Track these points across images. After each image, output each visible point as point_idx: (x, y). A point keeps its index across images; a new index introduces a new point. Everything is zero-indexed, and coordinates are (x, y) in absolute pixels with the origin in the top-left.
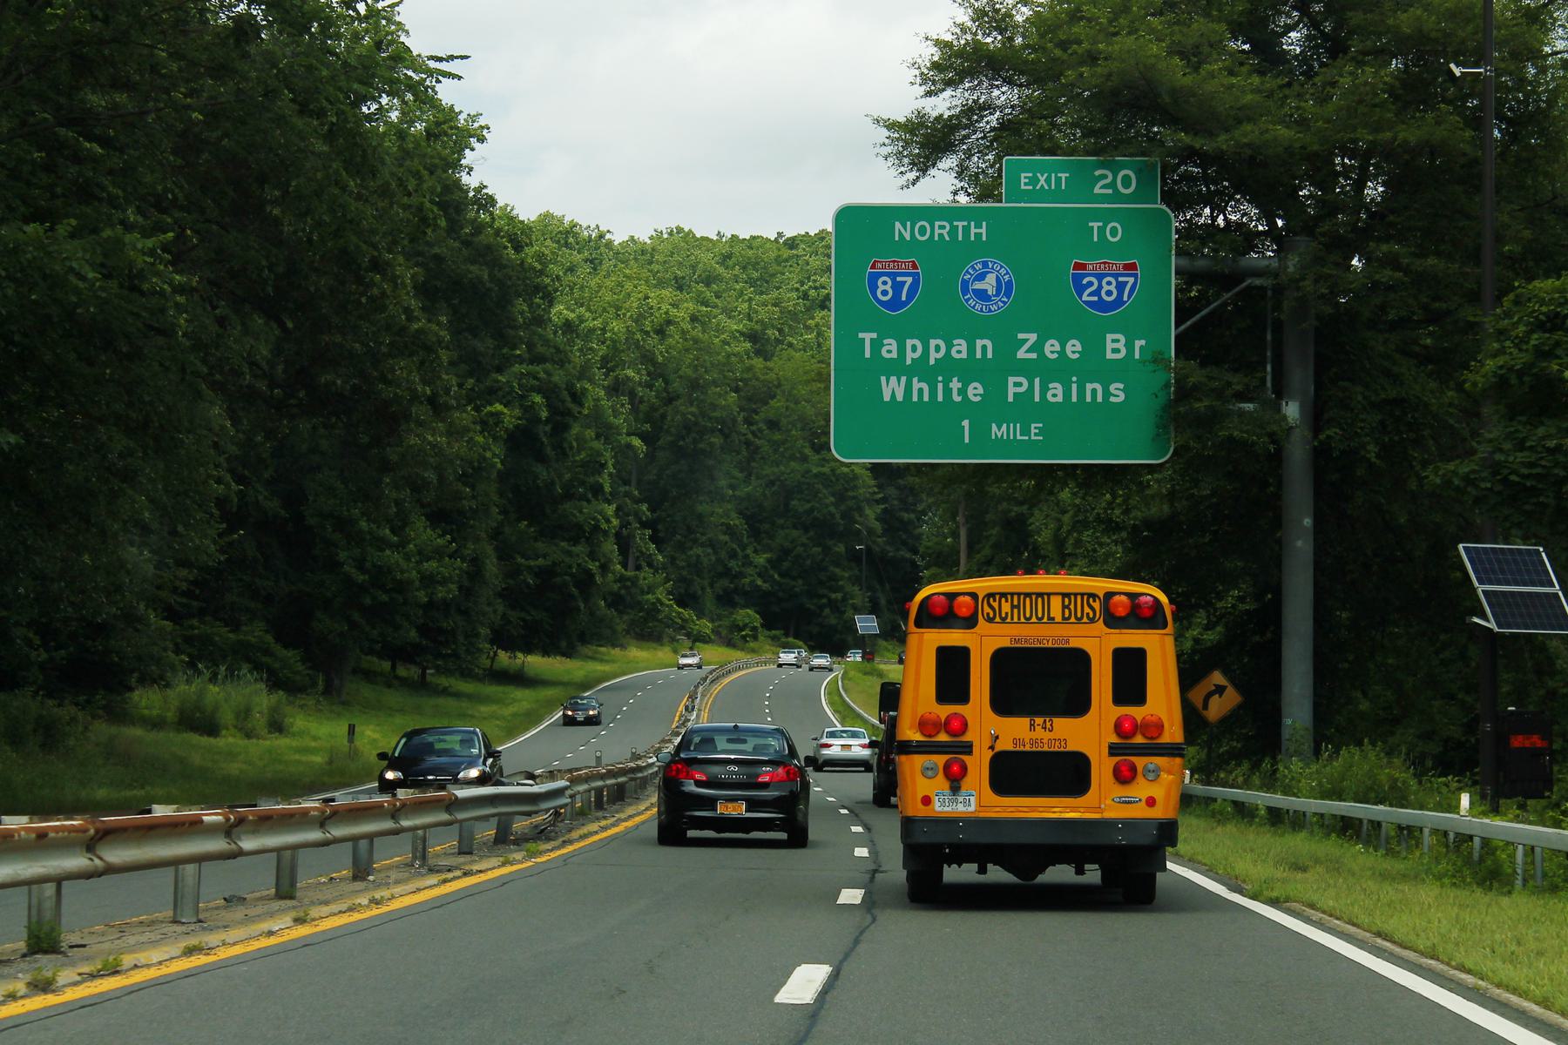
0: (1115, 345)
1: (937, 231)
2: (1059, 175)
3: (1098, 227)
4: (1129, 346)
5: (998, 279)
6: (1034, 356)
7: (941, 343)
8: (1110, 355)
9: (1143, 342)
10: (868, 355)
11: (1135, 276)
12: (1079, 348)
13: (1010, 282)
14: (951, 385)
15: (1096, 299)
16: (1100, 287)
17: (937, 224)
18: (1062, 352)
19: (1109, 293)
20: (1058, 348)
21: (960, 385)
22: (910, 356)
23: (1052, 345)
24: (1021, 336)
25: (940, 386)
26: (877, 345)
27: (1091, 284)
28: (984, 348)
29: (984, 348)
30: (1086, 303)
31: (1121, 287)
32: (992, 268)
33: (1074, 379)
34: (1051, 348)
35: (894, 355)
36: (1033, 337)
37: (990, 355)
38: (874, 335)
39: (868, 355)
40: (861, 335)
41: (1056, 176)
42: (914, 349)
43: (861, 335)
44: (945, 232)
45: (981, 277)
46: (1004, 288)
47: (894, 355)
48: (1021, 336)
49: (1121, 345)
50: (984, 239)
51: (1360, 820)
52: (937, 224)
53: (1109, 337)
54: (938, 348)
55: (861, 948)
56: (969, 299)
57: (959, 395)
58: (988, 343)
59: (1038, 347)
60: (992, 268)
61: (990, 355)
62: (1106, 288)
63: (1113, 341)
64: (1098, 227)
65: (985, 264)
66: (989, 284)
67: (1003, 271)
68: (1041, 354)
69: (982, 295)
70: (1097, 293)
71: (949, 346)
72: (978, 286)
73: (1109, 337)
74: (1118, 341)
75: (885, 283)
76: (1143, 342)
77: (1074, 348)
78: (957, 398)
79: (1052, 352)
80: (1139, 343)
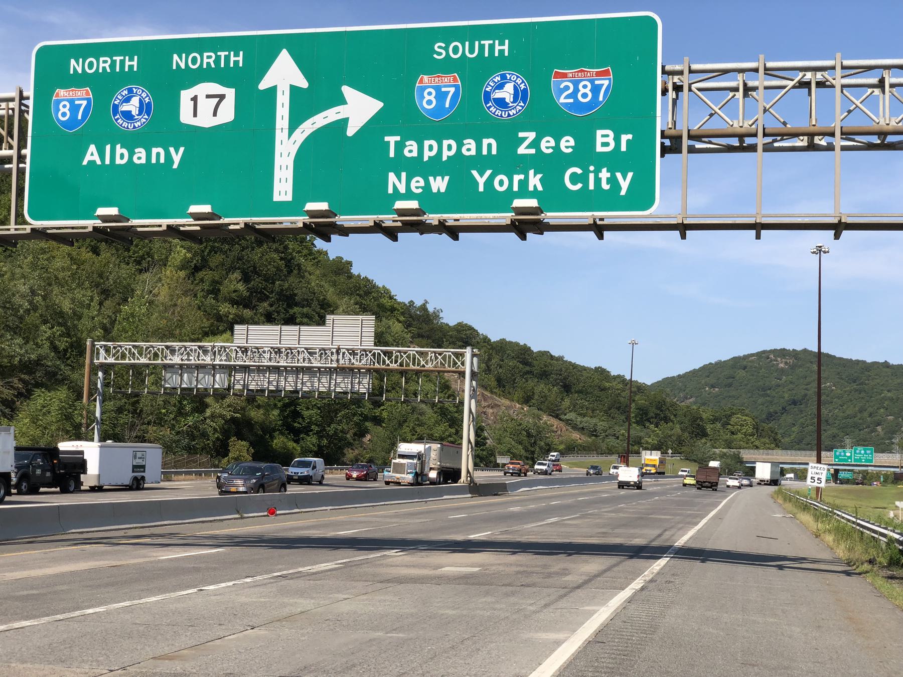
0: (605, 140)
1: (205, 60)
2: (482, 42)
3: (489, 44)
4: (617, 140)
6: (533, 151)
7: (453, 143)
8: (599, 149)
9: (630, 137)
10: (392, 155)
12: (572, 142)
13: (525, 90)
14: (600, 175)
15: (571, 101)
16: (576, 90)
17: (206, 54)
18: (557, 147)
19: (585, 95)
20: (552, 143)
21: (609, 175)
22: (427, 154)
24: (521, 135)
25: (592, 176)
26: (400, 146)
27: (567, 88)
28: (490, 145)
30: (566, 104)
31: (596, 90)
32: (510, 79)
33: (592, 168)
34: (547, 144)
35: (415, 154)
36: (532, 136)
37: (494, 152)
38: (398, 138)
39: (392, 155)
40: (387, 139)
41: (479, 43)
42: (431, 148)
43: (387, 139)
44: (211, 61)
46: (144, 108)
47: (415, 154)
48: (521, 135)
49: (611, 140)
50: (241, 65)
52: (206, 54)
53: (599, 133)
54: (450, 147)
55: (608, 574)
59: (535, 144)
61: (494, 152)
62: (582, 91)
63: (603, 136)
64: (489, 44)
66: (507, 93)
67: (144, 95)
69: (128, 115)
70: (574, 95)
71: (460, 145)
73: (599, 133)
74: (607, 136)
75: (430, 94)
76: (630, 137)
77: (567, 143)
78: (605, 186)
80: (625, 138)
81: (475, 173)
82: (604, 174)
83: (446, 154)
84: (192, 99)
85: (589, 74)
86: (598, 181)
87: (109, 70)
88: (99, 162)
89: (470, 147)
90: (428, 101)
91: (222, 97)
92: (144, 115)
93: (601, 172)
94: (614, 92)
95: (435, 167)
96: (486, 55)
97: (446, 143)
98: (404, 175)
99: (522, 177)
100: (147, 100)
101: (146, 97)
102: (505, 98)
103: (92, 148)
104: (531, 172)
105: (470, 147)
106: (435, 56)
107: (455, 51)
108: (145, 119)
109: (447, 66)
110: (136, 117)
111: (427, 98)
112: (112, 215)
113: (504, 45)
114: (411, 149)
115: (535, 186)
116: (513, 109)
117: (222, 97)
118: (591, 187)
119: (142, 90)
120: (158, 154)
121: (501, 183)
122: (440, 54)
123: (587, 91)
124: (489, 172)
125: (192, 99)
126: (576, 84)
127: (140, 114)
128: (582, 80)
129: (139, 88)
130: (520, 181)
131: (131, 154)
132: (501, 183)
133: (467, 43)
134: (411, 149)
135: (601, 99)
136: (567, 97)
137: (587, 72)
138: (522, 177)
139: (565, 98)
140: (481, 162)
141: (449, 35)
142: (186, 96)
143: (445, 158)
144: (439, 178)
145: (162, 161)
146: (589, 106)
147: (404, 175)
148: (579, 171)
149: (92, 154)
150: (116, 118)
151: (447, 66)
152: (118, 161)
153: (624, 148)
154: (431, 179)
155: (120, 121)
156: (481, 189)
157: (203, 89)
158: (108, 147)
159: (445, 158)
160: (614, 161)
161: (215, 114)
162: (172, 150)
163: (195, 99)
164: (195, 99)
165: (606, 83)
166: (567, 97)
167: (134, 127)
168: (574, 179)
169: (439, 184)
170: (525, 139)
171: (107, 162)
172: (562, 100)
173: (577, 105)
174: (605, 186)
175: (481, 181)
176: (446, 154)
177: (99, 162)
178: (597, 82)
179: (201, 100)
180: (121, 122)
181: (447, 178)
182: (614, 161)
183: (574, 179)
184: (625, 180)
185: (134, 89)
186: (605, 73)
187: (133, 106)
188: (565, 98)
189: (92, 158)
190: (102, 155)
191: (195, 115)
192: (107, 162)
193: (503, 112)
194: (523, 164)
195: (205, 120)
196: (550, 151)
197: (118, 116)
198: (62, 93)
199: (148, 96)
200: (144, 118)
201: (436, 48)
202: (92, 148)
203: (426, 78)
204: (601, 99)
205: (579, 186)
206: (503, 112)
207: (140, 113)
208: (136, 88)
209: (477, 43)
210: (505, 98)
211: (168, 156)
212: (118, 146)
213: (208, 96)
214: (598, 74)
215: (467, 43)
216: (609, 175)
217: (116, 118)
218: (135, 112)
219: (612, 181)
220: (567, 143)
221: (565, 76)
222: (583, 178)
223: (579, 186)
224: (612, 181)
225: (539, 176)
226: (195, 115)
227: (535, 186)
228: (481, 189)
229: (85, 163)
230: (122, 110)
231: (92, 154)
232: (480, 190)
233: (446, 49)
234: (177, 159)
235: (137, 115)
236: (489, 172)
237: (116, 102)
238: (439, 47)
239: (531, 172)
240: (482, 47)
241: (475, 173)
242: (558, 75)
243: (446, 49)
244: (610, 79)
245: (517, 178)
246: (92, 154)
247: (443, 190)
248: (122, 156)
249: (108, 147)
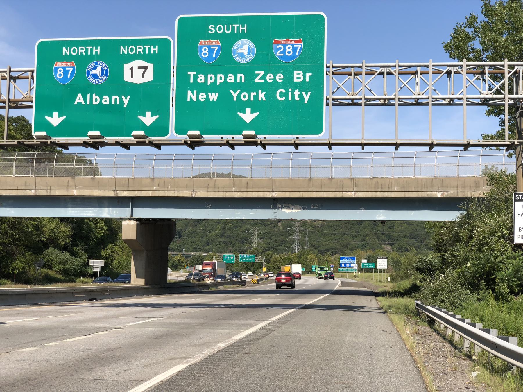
0: (299, 76)
2: (233, 25)
3: (237, 26)
5: (102, 69)
6: (262, 81)
8: (296, 80)
9: (311, 74)
10: (192, 81)
11: (301, 45)
12: (282, 77)
13: (107, 70)
14: (295, 93)
15: (282, 55)
16: (285, 50)
18: (274, 79)
19: (289, 52)
20: (272, 77)
22: (209, 82)
23: (270, 76)
24: (257, 72)
25: (290, 94)
26: (195, 77)
27: (280, 48)
28: (241, 78)
29: (241, 78)
30: (279, 56)
31: (294, 50)
32: (100, 65)
33: (290, 90)
34: (270, 77)
35: (203, 81)
36: (262, 73)
38: (195, 73)
39: (192, 81)
40: (189, 73)
41: (232, 26)
42: (211, 78)
43: (189, 73)
44: (83, 51)
45: (95, 68)
46: (104, 72)
47: (203, 81)
48: (257, 72)
49: (301, 76)
50: (246, 32)
51: (365, 272)
53: (296, 72)
54: (221, 78)
56: (90, 78)
57: (298, 98)
58: (242, 76)
59: (263, 77)
60: (100, 65)
61: (243, 81)
62: (288, 50)
63: (298, 74)
64: (237, 26)
65: (96, 63)
67: (104, 66)
68: (265, 80)
69: (95, 76)
70: (284, 52)
71: (226, 77)
72: (94, 72)
73: (296, 72)
74: (300, 74)
76: (311, 74)
77: (280, 77)
78: (297, 99)
79: (270, 79)
80: (308, 75)
81: (232, 91)
82: (297, 93)
83: (219, 82)
84: (130, 69)
85: (291, 42)
86: (293, 96)
87: (84, 54)
88: (83, 103)
89: (231, 78)
90: (204, 53)
91: (146, 68)
92: (104, 76)
93: (295, 92)
94: (304, 52)
95: (214, 88)
96: (236, 32)
97: (219, 76)
98: (195, 92)
99: (255, 93)
100: (106, 68)
101: (105, 67)
102: (243, 53)
103: (80, 95)
104: (260, 91)
105: (231, 78)
106: (209, 31)
107: (220, 29)
108: (105, 78)
109: (215, 36)
110: (100, 77)
111: (204, 52)
112: (97, 135)
113: (244, 27)
114: (201, 79)
115: (262, 98)
116: (248, 58)
117: (146, 68)
118: (290, 99)
119: (103, 63)
120: (116, 99)
121: (245, 96)
122: (212, 31)
123: (290, 50)
124: (238, 91)
125: (130, 69)
126: (285, 46)
127: (102, 75)
128: (288, 45)
129: (101, 62)
130: (254, 96)
131: (101, 99)
132: (245, 96)
133: (226, 26)
134: (201, 79)
135: (297, 54)
136: (280, 53)
137: (291, 40)
138: (255, 93)
139: (279, 53)
140: (235, 86)
141: (216, 21)
142: (127, 67)
143: (218, 84)
144: (213, 94)
145: (118, 103)
146: (291, 58)
147: (195, 92)
148: (284, 91)
149: (80, 99)
150: (89, 77)
151: (215, 36)
152: (94, 103)
153: (307, 80)
154: (209, 94)
155: (91, 79)
156: (235, 99)
157: (136, 63)
158: (89, 95)
159: (218, 84)
160: (302, 86)
161: (143, 77)
162: (123, 97)
163: (132, 69)
164: (132, 69)
165: (300, 46)
166: (280, 53)
167: (99, 82)
168: (281, 95)
169: (214, 97)
170: (259, 74)
171: (88, 103)
172: (278, 54)
173: (285, 57)
174: (297, 99)
175: (235, 95)
176: (219, 82)
177: (83, 103)
178: (295, 46)
179: (135, 70)
180: (92, 80)
181: (217, 94)
182: (302, 86)
183: (281, 95)
184: (307, 96)
185: (98, 62)
186: (299, 42)
187: (98, 71)
188: (279, 53)
189: (80, 101)
190: (85, 99)
191: (132, 77)
192: (88, 103)
193: (243, 60)
194: (257, 87)
195: (138, 79)
196: (271, 81)
197: (90, 77)
198: (59, 63)
199: (106, 66)
200: (104, 78)
201: (210, 27)
202: (80, 95)
203: (203, 42)
204: (297, 54)
205: (284, 98)
206: (243, 60)
207: (102, 75)
208: (99, 62)
209: (231, 26)
210: (243, 53)
211: (121, 100)
212: (94, 95)
213: (139, 68)
214: (296, 42)
215: (226, 26)
216: (299, 93)
217: (89, 77)
218: (99, 74)
219: (301, 96)
220: (280, 77)
221: (279, 42)
222: (286, 95)
223: (284, 98)
224: (301, 96)
225: (264, 93)
226: (132, 77)
227: (262, 98)
228: (235, 99)
229: (76, 103)
230: (92, 73)
231: (79, 99)
232: (234, 100)
233: (215, 28)
234: (126, 102)
235: (101, 76)
236: (238, 91)
237: (88, 69)
238: (212, 27)
239: (260, 91)
240: (233, 28)
241: (232, 91)
242: (276, 42)
243: (215, 28)
244: (301, 45)
245: (253, 94)
246: (80, 99)
247: (215, 100)
248: (96, 100)
249: (89, 95)
